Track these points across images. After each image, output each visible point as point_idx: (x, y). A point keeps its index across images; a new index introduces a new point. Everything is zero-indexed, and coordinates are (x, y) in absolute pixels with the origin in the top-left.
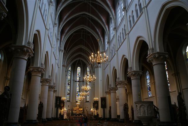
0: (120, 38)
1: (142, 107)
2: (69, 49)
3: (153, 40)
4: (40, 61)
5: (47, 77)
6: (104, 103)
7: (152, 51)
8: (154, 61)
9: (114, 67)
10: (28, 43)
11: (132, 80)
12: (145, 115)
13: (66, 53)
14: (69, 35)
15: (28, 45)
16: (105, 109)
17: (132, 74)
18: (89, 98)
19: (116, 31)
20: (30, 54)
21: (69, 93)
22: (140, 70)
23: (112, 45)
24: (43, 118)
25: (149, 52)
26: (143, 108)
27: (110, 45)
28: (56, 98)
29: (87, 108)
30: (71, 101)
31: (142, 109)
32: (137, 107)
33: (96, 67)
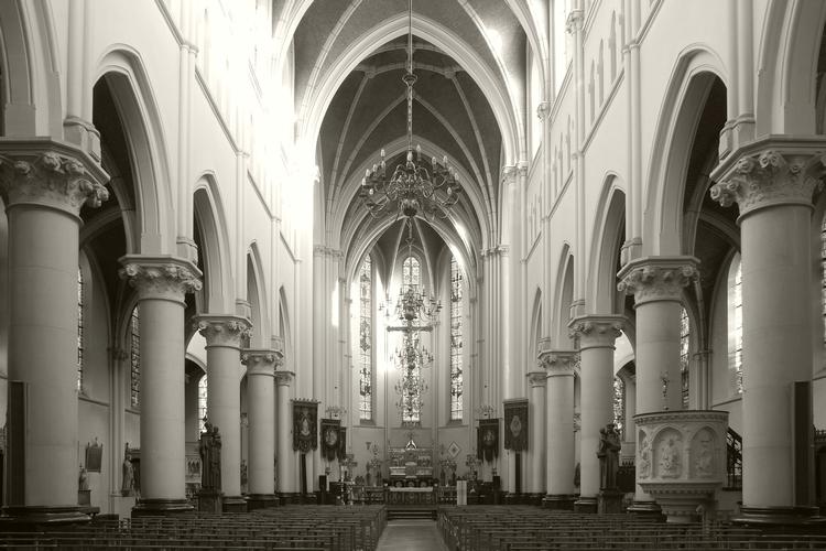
0: (597, 77)
1: (667, 439)
2: (337, 160)
3: (758, 64)
4: (164, 229)
5: (228, 309)
6: (520, 427)
7: (740, 134)
8: (749, 193)
9: (566, 247)
10: (65, 125)
11: (638, 306)
12: (676, 477)
13: (336, 185)
14: (340, 72)
15: (67, 139)
16: (524, 454)
17: (639, 278)
18: (460, 408)
19: (584, 33)
20: (87, 189)
21: (367, 388)
22: (685, 252)
23: (561, 125)
24: (226, 495)
25: (723, 139)
26: (671, 444)
27: (550, 125)
28: (295, 407)
29: (454, 450)
30: (380, 422)
31: (667, 446)
32: (646, 439)
33: (489, 253)
